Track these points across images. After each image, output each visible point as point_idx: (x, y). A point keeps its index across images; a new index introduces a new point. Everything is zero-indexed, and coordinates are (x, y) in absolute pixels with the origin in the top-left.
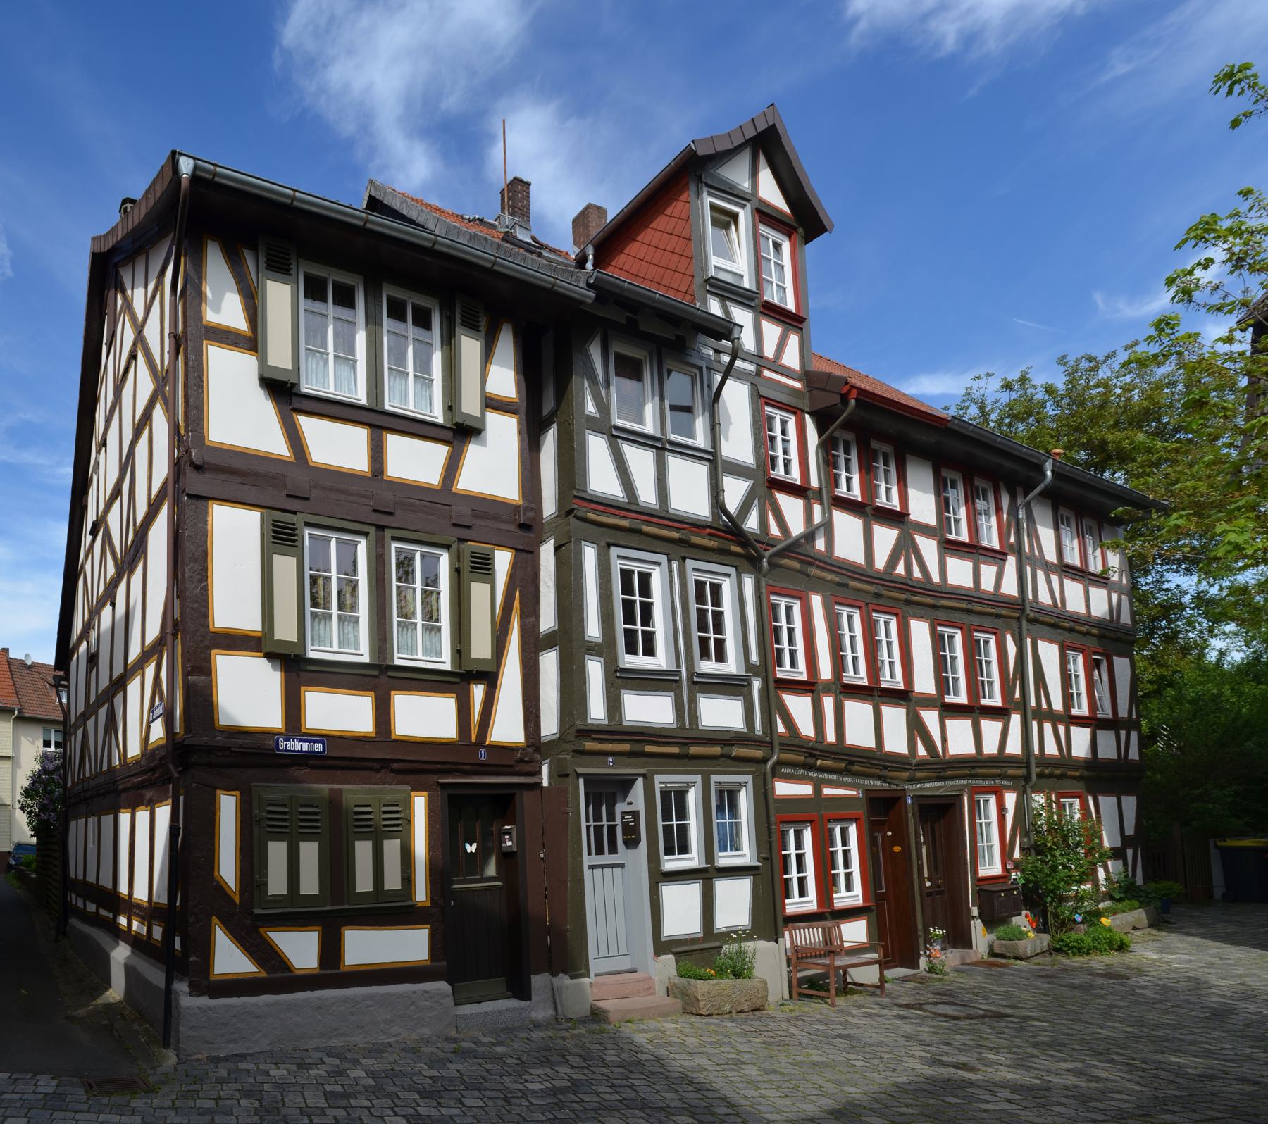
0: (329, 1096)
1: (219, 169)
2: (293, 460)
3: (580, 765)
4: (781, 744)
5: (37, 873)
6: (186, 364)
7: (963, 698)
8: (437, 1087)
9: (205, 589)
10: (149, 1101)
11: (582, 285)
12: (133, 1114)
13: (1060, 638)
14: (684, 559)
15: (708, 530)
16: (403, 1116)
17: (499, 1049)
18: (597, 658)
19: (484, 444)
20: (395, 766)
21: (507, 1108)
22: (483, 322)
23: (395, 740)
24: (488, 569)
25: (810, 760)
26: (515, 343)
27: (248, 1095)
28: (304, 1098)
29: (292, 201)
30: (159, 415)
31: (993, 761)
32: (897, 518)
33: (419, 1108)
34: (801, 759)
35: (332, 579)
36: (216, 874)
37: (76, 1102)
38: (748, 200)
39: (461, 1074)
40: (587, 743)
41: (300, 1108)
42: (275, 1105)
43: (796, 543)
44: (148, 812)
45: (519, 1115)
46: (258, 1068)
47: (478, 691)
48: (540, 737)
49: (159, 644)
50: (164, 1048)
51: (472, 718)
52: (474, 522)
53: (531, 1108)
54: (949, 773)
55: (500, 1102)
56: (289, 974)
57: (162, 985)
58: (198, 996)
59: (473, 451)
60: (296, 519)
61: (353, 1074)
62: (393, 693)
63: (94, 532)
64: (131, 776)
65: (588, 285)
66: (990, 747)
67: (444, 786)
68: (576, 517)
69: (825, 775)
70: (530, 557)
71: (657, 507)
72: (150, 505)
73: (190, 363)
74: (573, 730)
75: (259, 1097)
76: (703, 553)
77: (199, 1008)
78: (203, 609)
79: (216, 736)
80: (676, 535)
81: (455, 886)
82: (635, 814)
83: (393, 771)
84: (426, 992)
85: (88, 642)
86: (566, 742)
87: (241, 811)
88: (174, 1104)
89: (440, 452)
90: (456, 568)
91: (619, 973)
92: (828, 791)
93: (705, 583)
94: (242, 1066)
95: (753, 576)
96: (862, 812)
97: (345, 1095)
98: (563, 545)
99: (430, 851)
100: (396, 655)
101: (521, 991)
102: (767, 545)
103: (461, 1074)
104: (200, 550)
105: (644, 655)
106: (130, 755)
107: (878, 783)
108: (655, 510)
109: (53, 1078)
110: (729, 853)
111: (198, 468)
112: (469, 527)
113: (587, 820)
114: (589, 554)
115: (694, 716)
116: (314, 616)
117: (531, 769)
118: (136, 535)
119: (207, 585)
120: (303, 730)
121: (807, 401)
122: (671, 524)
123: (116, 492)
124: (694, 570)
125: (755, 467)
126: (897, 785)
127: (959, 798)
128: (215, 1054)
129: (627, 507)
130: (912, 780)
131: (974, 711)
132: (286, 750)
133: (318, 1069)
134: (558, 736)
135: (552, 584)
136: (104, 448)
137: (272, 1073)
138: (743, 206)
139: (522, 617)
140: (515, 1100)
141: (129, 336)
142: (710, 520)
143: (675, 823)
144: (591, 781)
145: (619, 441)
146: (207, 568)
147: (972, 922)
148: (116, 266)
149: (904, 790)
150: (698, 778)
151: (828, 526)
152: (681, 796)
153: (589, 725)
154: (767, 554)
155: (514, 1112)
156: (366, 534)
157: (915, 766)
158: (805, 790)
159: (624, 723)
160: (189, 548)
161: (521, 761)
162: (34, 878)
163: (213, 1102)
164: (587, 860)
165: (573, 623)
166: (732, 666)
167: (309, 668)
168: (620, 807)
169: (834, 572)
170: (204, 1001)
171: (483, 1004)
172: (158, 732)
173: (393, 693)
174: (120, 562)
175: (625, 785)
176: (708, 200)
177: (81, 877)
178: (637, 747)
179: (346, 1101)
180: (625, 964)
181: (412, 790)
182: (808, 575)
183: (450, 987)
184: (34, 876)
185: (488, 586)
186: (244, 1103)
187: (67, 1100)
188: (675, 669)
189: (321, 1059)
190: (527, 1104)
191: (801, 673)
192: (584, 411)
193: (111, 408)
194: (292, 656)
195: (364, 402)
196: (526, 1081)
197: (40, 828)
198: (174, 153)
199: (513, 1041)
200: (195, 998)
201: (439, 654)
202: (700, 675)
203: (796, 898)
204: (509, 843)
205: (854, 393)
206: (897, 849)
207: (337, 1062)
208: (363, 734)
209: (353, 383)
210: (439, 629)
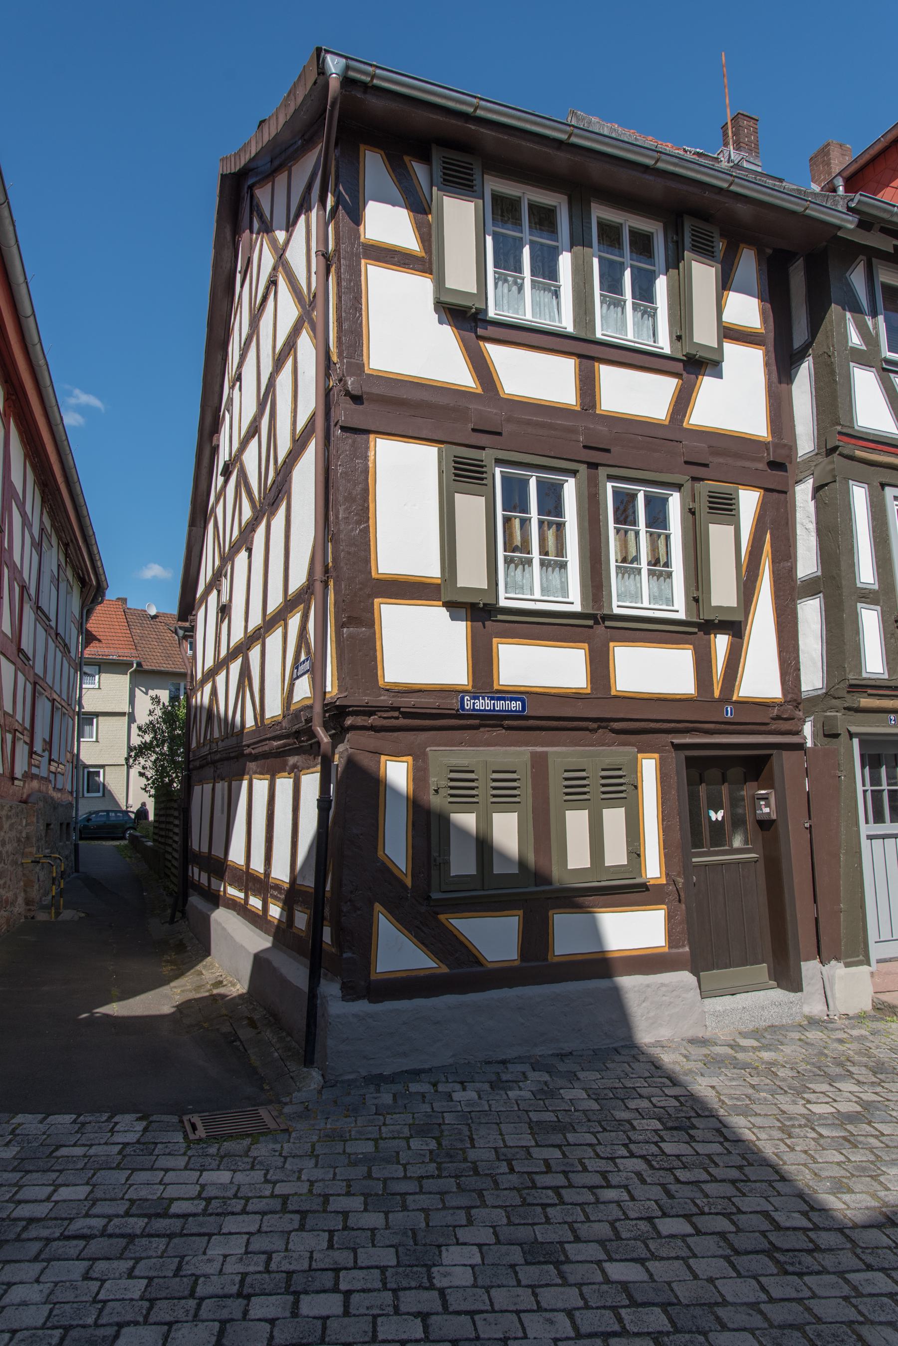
0: (534, 1128)
1: (378, 71)
2: (479, 391)
3: (854, 724)
5: (154, 841)
6: (339, 284)
8: (687, 1112)
9: (366, 531)
10: (278, 1147)
12: (252, 1168)
16: (642, 1157)
17: (766, 1055)
18: (872, 607)
19: (719, 375)
20: (616, 725)
21: (788, 1141)
22: (720, 246)
23: (615, 697)
24: (731, 510)
27: (421, 1131)
28: (501, 1134)
29: (475, 110)
30: (306, 347)
33: (662, 1145)
35: (532, 520)
36: (380, 853)
37: (169, 1154)
39: (717, 1092)
40: (862, 700)
41: (495, 1149)
42: (459, 1146)
44: (292, 780)
45: (805, 1152)
46: (436, 1091)
47: (721, 643)
48: (800, 691)
49: (306, 593)
50: (305, 1066)
52: (711, 459)
53: (822, 1141)
55: (777, 1134)
56: (479, 969)
57: (306, 988)
58: (353, 1001)
59: (707, 383)
60: (483, 455)
61: (567, 1094)
63: (227, 473)
64: (269, 739)
65: (849, 209)
67: (677, 747)
68: (840, 455)
70: (782, 496)
72: (294, 441)
73: (344, 284)
74: (845, 685)
75: (437, 1134)
77: (355, 1016)
78: (796, 689)
79: (381, 695)
81: (694, 860)
84: (663, 985)
85: (219, 592)
86: (835, 698)
87: (414, 779)
88: (313, 1150)
89: (666, 386)
90: (690, 509)
94: (414, 1087)
97: (560, 1127)
98: (826, 485)
99: (663, 820)
100: (615, 603)
103: (717, 1092)
104: (359, 488)
106: (268, 715)
109: (139, 1119)
111: (357, 399)
112: (706, 465)
113: (864, 785)
116: (508, 561)
117: (791, 728)
118: (277, 473)
119: (368, 526)
120: (496, 687)
123: (252, 430)
128: (376, 1071)
132: (474, 709)
133: (520, 1089)
134: (824, 691)
136: (238, 384)
137: (456, 1096)
139: (775, 562)
140: (797, 1130)
141: (269, 260)
144: (866, 741)
145: (892, 375)
146: (368, 508)
148: (251, 188)
153: (865, 679)
155: (797, 1148)
156: (574, 473)
160: (341, 487)
161: (778, 718)
162: (149, 847)
163: (371, 1143)
164: (865, 829)
165: (842, 568)
167: (500, 617)
170: (362, 1006)
171: (738, 996)
172: (303, 689)
173: (612, 644)
174: (258, 504)
177: (205, 849)
179: (561, 1136)
181: (639, 752)
183: (694, 979)
184: (150, 844)
185: (731, 528)
186: (415, 1143)
187: (156, 1152)
189: (524, 1073)
190: (814, 1135)
192: (847, 342)
193: (250, 344)
194: (481, 606)
195: (570, 329)
196: (809, 1102)
197: (162, 793)
198: (319, 50)
199: (782, 1044)
200: (350, 1003)
201: (671, 601)
204: (767, 810)
207: (546, 1077)
208: (574, 691)
209: (556, 310)
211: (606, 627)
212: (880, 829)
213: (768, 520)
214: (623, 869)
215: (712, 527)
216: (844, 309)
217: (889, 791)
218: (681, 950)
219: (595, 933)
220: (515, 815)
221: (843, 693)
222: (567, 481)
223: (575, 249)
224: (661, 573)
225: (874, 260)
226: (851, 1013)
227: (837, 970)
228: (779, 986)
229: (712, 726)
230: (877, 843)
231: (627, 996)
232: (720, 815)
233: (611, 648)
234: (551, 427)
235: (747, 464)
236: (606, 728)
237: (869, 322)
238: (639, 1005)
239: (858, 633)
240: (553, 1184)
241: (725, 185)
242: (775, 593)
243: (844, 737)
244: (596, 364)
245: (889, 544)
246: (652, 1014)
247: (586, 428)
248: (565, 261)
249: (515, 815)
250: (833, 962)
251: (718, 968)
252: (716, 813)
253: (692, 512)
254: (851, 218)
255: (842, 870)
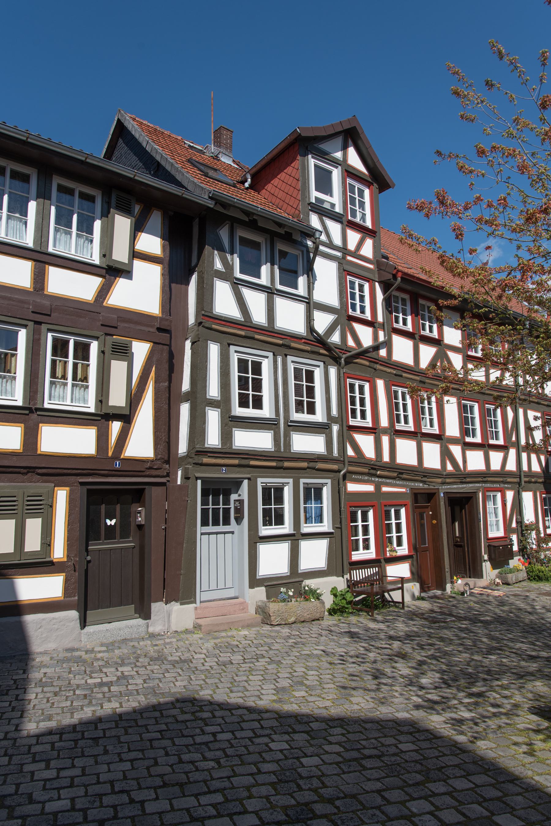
4: (349, 462)
7: (478, 439)
11: (206, 197)
13: (542, 410)
14: (286, 355)
15: (303, 341)
18: (215, 409)
19: (130, 278)
20: (40, 471)
22: (137, 209)
23: (40, 455)
25: (372, 471)
26: (163, 223)
31: (496, 474)
32: (437, 342)
34: (366, 470)
38: (340, 165)
40: (204, 459)
43: (367, 351)
48: (178, 454)
51: (110, 441)
54: (468, 480)
59: (121, 283)
62: (41, 425)
65: (210, 197)
66: (496, 465)
67: (82, 484)
68: (203, 326)
69: (384, 480)
71: (267, 325)
76: (300, 352)
80: (281, 342)
82: (241, 502)
83: (38, 474)
84: (54, 619)
89: (94, 283)
91: (214, 600)
92: (385, 489)
93: (303, 369)
95: (336, 368)
96: (409, 501)
99: (68, 525)
101: (146, 614)
102: (346, 351)
105: (253, 408)
107: (421, 485)
108: (265, 327)
110: (314, 524)
112: (116, 328)
114: (214, 350)
115: (288, 444)
117: (159, 473)
121: (377, 276)
122: (276, 335)
124: (293, 362)
125: (339, 308)
126: (434, 486)
127: (475, 494)
129: (243, 324)
130: (443, 483)
131: (484, 447)
134: (186, 454)
135: (189, 364)
138: (337, 168)
139: (156, 382)
142: (305, 335)
143: (273, 506)
145: (240, 286)
147: (484, 564)
149: (438, 489)
150: (291, 481)
151: (388, 344)
152: (279, 491)
153: (206, 448)
154: (344, 356)
156: (25, 326)
157: (446, 475)
158: (370, 488)
159: (234, 447)
161: (150, 468)
164: (200, 529)
166: (319, 417)
168: (234, 497)
169: (392, 368)
173: (41, 425)
175: (237, 484)
176: (312, 162)
178: (244, 462)
180: (231, 593)
182: (375, 369)
185: (125, 364)
188: (274, 417)
191: (368, 422)
192: (213, 267)
195: (31, 245)
201: (85, 401)
202: (292, 422)
203: (361, 550)
205: (400, 274)
206: (434, 522)
208: (11, 451)
210: (87, 387)
211: (38, 415)
212: (206, 529)
213: (155, 359)
214: (37, 553)
215: (113, 362)
216: (213, 249)
217: (223, 508)
218: (73, 599)
219: (13, 590)
220: (13, 521)
221: (193, 456)
222: (20, 330)
223: (39, 200)
224: (82, 386)
225: (235, 224)
226: (179, 630)
227: (175, 607)
228: (140, 617)
229: (106, 472)
230: (205, 537)
231: (28, 625)
232: (113, 522)
233: (40, 427)
234: (10, 299)
235: (143, 328)
236: (34, 472)
237: (229, 257)
238: (36, 630)
239: (204, 423)
240: (204, 741)
241: (132, 176)
242: (155, 399)
243: (192, 479)
244: (47, 266)
245: (230, 376)
246: (44, 635)
247: (34, 301)
248: (32, 206)
249: (13, 521)
250: (173, 603)
251: (102, 608)
252: (111, 521)
253: (103, 352)
254: (210, 202)
255: (184, 552)
